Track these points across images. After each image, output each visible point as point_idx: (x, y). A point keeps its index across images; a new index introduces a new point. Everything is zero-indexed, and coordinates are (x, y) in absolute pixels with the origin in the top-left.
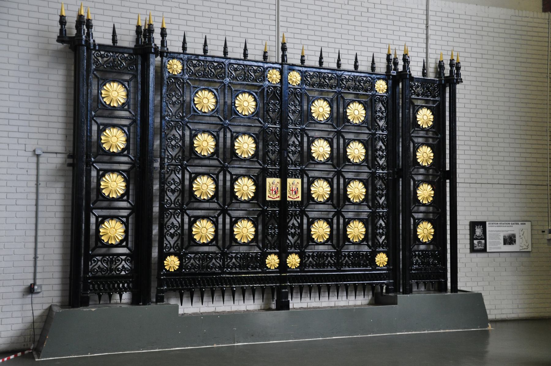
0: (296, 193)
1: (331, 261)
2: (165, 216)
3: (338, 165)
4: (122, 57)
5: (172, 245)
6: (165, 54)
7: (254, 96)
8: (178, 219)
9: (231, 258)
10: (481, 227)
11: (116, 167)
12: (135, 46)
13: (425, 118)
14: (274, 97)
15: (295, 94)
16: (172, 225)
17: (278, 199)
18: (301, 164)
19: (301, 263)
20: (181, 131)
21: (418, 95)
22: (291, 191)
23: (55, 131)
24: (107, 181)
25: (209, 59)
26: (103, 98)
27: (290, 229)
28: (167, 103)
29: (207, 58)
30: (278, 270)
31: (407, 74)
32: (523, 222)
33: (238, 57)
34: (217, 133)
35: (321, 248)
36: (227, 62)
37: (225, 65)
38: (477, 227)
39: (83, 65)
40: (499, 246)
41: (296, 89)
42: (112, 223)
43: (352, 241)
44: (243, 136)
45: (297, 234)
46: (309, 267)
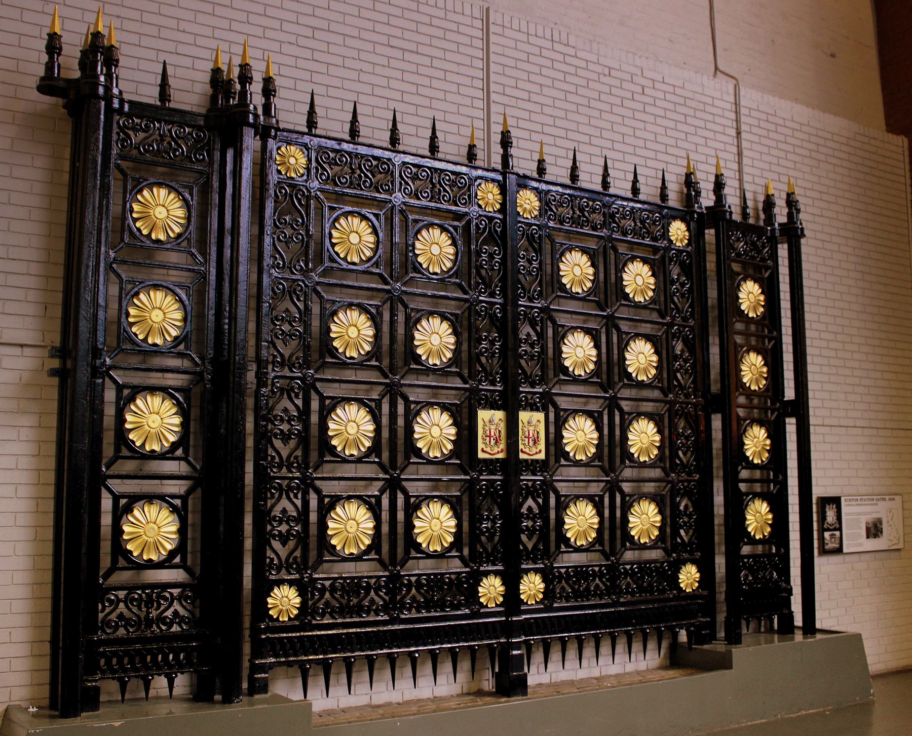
0: (535, 443)
1: (376, 598)
2: (269, 495)
3: (393, 369)
4: (180, 133)
5: (283, 559)
6: (273, 132)
7: (451, 233)
8: (295, 500)
9: (323, 590)
10: (834, 506)
11: (155, 379)
12: (209, 110)
13: (639, 281)
14: (491, 239)
15: (531, 239)
16: (283, 515)
17: (501, 456)
18: (543, 380)
19: (303, 608)
20: (303, 303)
21: (625, 234)
22: (527, 439)
23: (18, 294)
24: (140, 413)
25: (362, 150)
26: (135, 220)
27: (275, 524)
28: (273, 238)
29: (359, 147)
30: (502, 609)
31: (726, 211)
32: (891, 497)
33: (420, 152)
34: (377, 309)
35: (349, 570)
36: (398, 159)
37: (394, 165)
38: (828, 507)
39: (97, 139)
40: (859, 541)
41: (531, 225)
42: (149, 512)
43: (573, 544)
44: (430, 319)
45: (293, 535)
46: (323, 616)
